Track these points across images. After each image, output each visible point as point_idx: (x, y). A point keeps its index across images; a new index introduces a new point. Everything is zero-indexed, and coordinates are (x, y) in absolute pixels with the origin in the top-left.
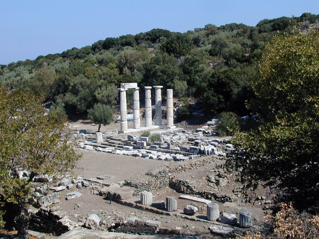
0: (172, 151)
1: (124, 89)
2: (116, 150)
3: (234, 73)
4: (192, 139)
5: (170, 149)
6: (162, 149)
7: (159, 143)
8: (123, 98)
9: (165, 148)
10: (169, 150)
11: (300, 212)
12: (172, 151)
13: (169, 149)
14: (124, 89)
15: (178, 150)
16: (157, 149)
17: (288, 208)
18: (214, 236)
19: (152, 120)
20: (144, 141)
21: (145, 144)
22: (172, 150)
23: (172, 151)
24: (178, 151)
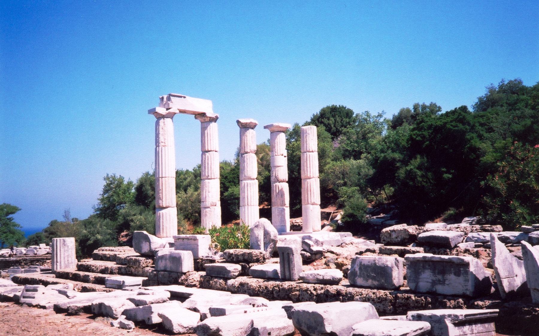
0: (304, 286)
1: (167, 109)
2: (35, 290)
3: (492, 118)
4: (403, 236)
5: (296, 277)
6: (253, 282)
7: (244, 255)
8: (162, 135)
9: (111, 258)
10: (286, 284)
11: (135, 198)
12: (304, 286)
13: (290, 279)
14: (167, 109)
15: (335, 282)
16: (230, 282)
17: (249, 246)
18: (347, 287)
19: (173, 121)
20: (184, 249)
21: (188, 264)
22: (304, 280)
23: (301, 290)
24: (332, 289)
